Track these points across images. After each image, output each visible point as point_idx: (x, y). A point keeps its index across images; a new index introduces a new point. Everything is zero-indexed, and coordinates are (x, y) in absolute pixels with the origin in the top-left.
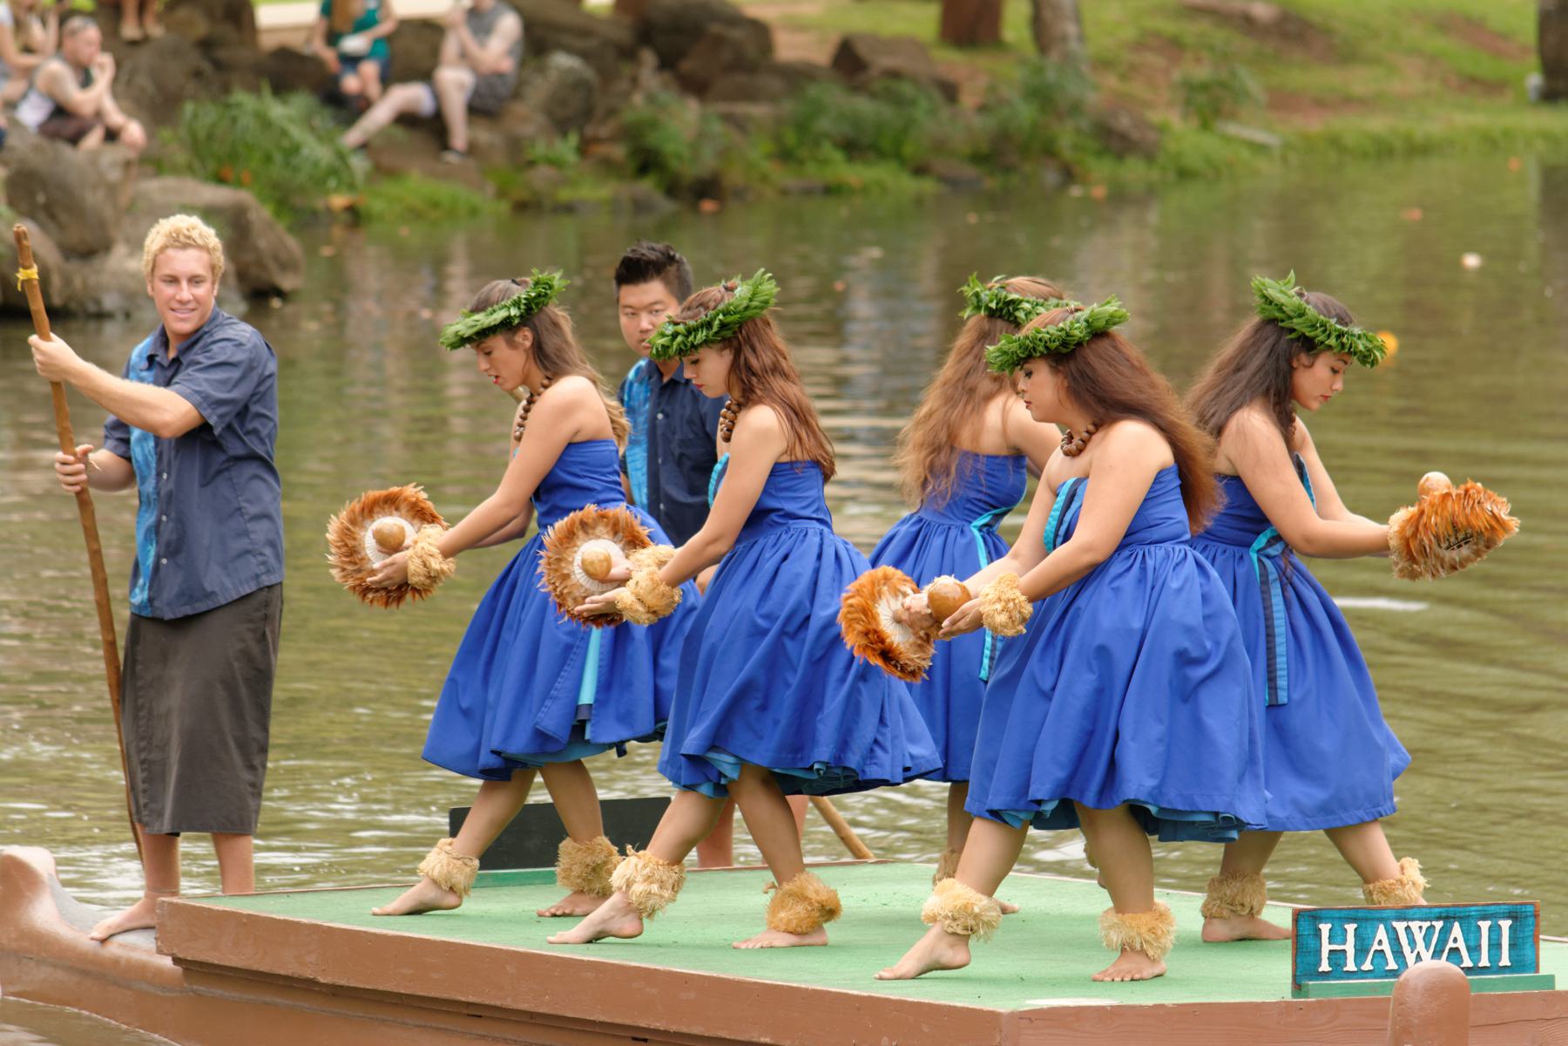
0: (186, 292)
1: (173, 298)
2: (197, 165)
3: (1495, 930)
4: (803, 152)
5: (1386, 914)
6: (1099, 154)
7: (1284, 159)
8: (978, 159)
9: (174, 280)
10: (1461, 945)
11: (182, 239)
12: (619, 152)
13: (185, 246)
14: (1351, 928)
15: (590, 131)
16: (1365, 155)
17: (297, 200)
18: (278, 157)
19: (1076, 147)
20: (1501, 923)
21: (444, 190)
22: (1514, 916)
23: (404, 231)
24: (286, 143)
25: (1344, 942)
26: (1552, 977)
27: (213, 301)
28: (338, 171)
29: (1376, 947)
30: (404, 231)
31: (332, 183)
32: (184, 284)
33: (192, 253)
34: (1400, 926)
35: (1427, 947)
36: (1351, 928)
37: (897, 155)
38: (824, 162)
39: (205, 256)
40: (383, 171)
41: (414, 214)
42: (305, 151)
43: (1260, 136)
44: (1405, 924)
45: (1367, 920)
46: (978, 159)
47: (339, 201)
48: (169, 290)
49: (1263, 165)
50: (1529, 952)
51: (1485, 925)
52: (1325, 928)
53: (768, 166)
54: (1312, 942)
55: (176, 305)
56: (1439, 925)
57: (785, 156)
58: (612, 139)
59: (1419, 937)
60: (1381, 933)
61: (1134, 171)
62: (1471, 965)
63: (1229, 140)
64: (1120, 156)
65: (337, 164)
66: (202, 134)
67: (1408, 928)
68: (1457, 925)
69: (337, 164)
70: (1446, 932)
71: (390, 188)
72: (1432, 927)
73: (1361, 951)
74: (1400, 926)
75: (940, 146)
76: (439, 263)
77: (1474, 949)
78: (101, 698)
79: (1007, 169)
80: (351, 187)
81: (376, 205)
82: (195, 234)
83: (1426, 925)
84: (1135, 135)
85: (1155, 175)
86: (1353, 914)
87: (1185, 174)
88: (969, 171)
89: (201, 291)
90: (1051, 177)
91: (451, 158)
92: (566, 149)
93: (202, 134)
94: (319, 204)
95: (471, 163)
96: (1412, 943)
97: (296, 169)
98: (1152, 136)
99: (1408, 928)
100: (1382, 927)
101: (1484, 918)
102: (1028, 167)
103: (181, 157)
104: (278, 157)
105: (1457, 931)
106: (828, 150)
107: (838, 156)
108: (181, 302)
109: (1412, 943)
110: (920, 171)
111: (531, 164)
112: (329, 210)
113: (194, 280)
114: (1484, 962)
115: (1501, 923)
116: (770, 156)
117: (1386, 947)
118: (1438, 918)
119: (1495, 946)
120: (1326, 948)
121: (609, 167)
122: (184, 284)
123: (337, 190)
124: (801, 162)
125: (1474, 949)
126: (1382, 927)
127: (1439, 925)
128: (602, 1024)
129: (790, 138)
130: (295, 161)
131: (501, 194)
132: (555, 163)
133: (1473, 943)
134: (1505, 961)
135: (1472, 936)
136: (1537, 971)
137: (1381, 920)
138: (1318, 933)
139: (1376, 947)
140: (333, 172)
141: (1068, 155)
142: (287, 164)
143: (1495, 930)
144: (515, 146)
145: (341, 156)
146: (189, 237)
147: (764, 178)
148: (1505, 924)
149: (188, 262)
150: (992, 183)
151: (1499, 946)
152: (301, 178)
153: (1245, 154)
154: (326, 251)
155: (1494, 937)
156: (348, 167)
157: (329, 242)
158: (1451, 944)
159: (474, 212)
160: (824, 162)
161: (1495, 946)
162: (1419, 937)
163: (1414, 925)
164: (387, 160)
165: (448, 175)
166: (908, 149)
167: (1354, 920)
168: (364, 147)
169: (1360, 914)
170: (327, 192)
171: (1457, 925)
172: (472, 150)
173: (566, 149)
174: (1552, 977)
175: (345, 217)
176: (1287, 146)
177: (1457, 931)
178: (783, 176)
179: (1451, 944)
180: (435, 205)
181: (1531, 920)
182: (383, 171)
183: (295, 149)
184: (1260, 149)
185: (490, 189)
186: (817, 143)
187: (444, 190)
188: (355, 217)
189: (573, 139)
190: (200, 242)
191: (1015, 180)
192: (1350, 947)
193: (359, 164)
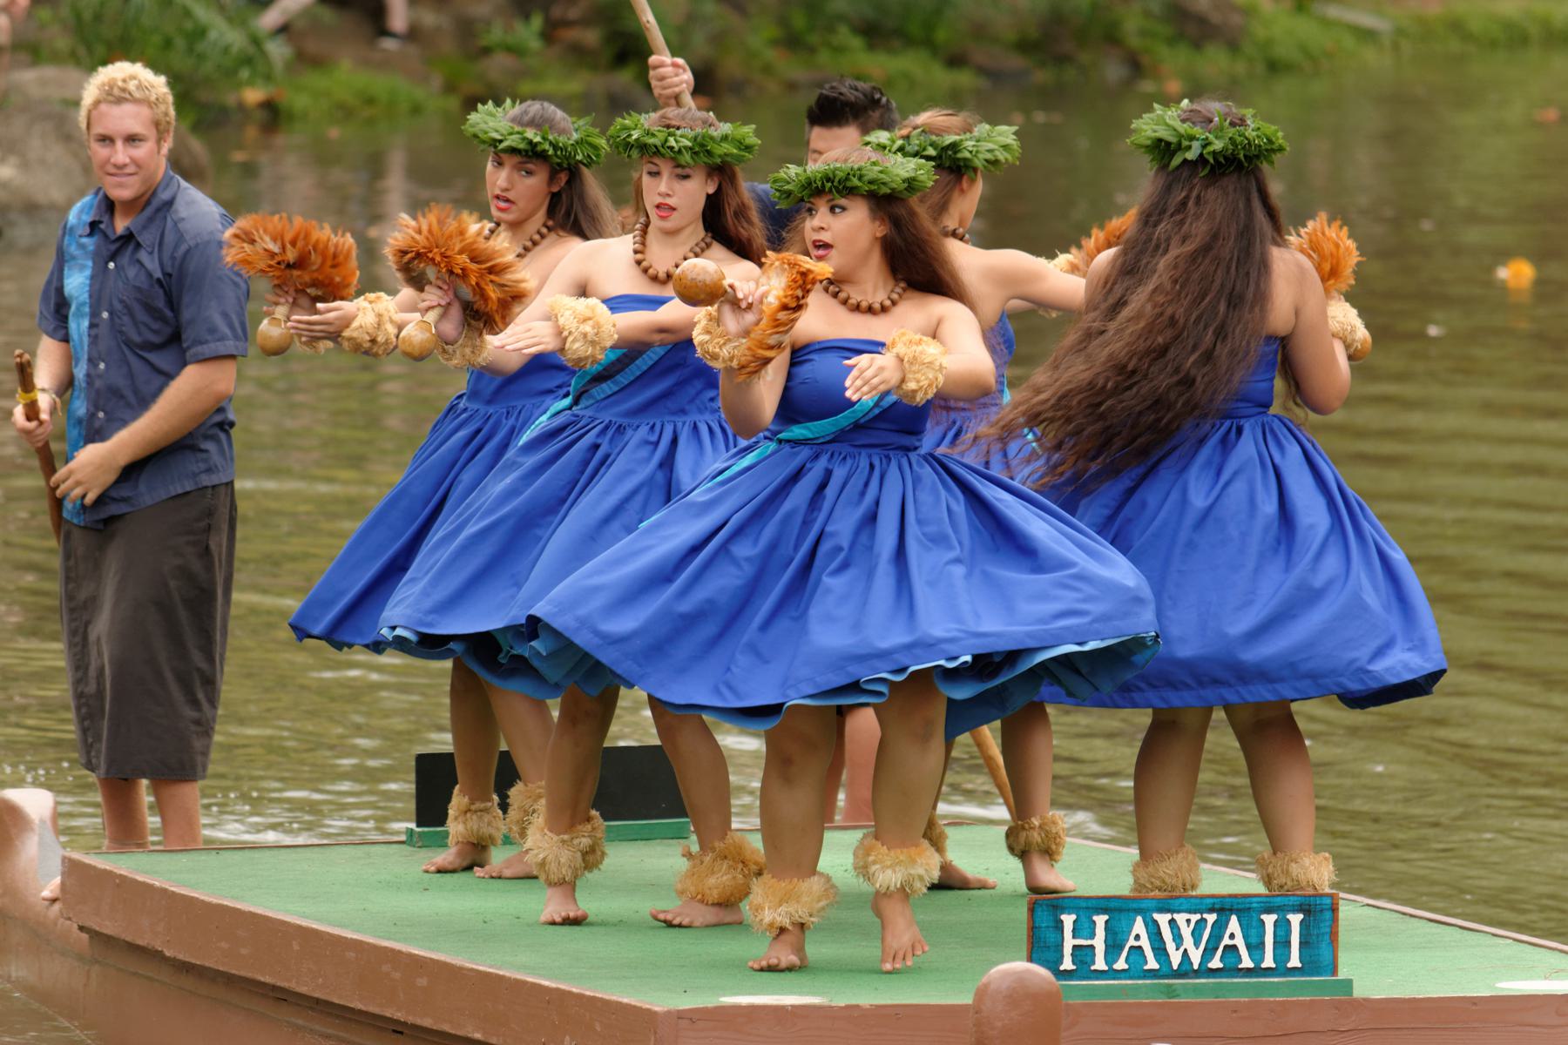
0: (121, 154)
1: (108, 161)
2: (82, 51)
3: (1282, 927)
4: (813, 39)
5: (1144, 904)
6: (1172, 41)
7: (1396, 47)
8: (1025, 46)
9: (106, 139)
10: (1239, 942)
11: (116, 92)
12: (591, 37)
13: (119, 101)
14: (1100, 920)
15: (557, 12)
16: (1493, 44)
17: (203, 95)
18: (180, 43)
19: (1144, 33)
20: (1290, 917)
21: (380, 83)
22: (1307, 909)
23: (334, 133)
24: (189, 25)
25: (1092, 936)
26: (1350, 981)
27: (163, 162)
28: (252, 60)
29: (1132, 942)
30: (334, 133)
31: (245, 74)
32: (119, 144)
33: (128, 108)
34: (1163, 919)
35: (1197, 945)
36: (1100, 920)
37: (927, 43)
38: (839, 50)
39: (145, 111)
40: (306, 60)
41: (344, 112)
42: (213, 35)
43: (1367, 20)
44: (1168, 916)
45: (1120, 910)
46: (1025, 46)
47: (253, 95)
48: (101, 151)
49: (1370, 55)
50: (1325, 951)
51: (1269, 920)
52: (1068, 920)
53: (771, 55)
54: (1051, 936)
55: (113, 170)
56: (1211, 918)
57: (792, 42)
58: (584, 22)
59: (1186, 932)
60: (1139, 926)
61: (1215, 62)
62: (1251, 965)
63: (1327, 23)
64: (1197, 45)
65: (251, 50)
66: (87, 15)
67: (1172, 922)
68: (1234, 918)
69: (251, 50)
70: (1220, 927)
71: (315, 79)
72: (1204, 920)
73: (1113, 948)
74: (1163, 919)
75: (980, 31)
76: (375, 167)
77: (1256, 947)
78: (1236, 773)
79: (1062, 60)
80: (268, 78)
81: (299, 101)
82: (132, 86)
83: (1195, 918)
84: (1216, 18)
85: (1240, 68)
86: (1103, 904)
87: (1275, 67)
88: (1015, 61)
89: (141, 151)
90: (1113, 71)
91: (389, 44)
92: (528, 33)
93: (87, 15)
94: (230, 99)
95: (412, 50)
96: (1178, 938)
97: (201, 57)
98: (1236, 19)
99: (1172, 922)
100: (1139, 919)
101: (1269, 911)
102: (1085, 57)
103: (62, 43)
104: (180, 43)
105: (1234, 925)
106: (844, 35)
107: (856, 42)
108: (115, 166)
109: (1178, 938)
110: (955, 61)
111: (486, 51)
112: (241, 107)
113: (132, 139)
114: (1269, 962)
115: (1290, 917)
116: (775, 43)
117: (1145, 943)
118: (1211, 911)
119: (1282, 944)
120: (1069, 943)
121: (579, 55)
122: (119, 144)
123: (250, 83)
124: (812, 50)
125: (1256, 947)
126: (1139, 919)
127: (1211, 918)
128: (361, 1012)
129: (799, 21)
130: (200, 47)
131: (450, 88)
132: (515, 51)
133: (1254, 940)
134: (1295, 962)
135: (1253, 932)
136: (1335, 972)
137: (1139, 911)
138: (1059, 926)
139: (1132, 942)
140: (247, 61)
141: (1134, 42)
142: (190, 50)
143: (1282, 927)
144: (467, 29)
145: (256, 41)
146: (124, 90)
147: (767, 69)
148: (1296, 919)
149: (128, 118)
150: (1042, 76)
151: (1288, 943)
152: (208, 68)
153: (1349, 42)
154: (239, 156)
155: (1281, 933)
156: (263, 53)
157: (240, 147)
158: (1226, 941)
159: (416, 110)
160: (839, 50)
161: (1282, 944)
162: (1186, 932)
163: (1181, 918)
164: (312, 46)
165: (386, 64)
166: (941, 35)
167: (1104, 911)
168: (284, 29)
169: (1112, 904)
170: (240, 85)
171: (1234, 918)
172: (413, 34)
173: (528, 33)
174: (1350, 981)
175: (260, 115)
176: (1400, 32)
177: (1234, 925)
178: (791, 68)
179: (1226, 941)
180: (370, 101)
181: (1328, 915)
182: (306, 60)
183: (200, 32)
184: (1367, 35)
185: (437, 81)
186: (830, 29)
187: (380, 83)
188: (273, 115)
189: (537, 22)
190: (137, 95)
191: (1070, 74)
192: (1099, 942)
193: (278, 51)
